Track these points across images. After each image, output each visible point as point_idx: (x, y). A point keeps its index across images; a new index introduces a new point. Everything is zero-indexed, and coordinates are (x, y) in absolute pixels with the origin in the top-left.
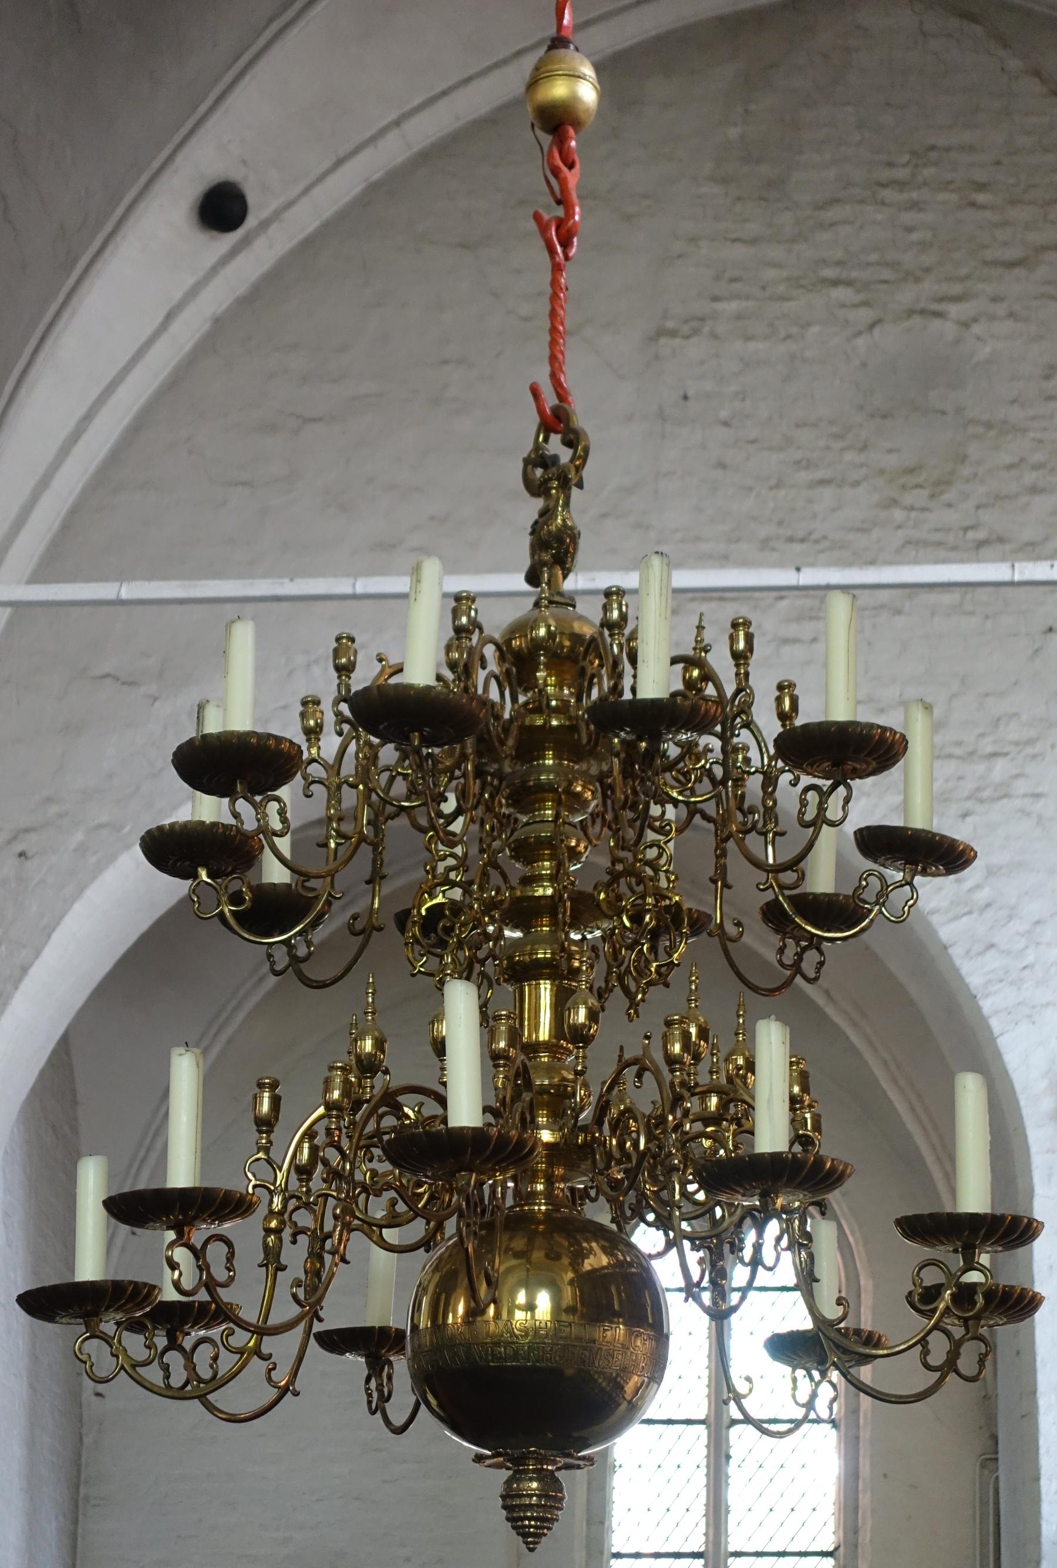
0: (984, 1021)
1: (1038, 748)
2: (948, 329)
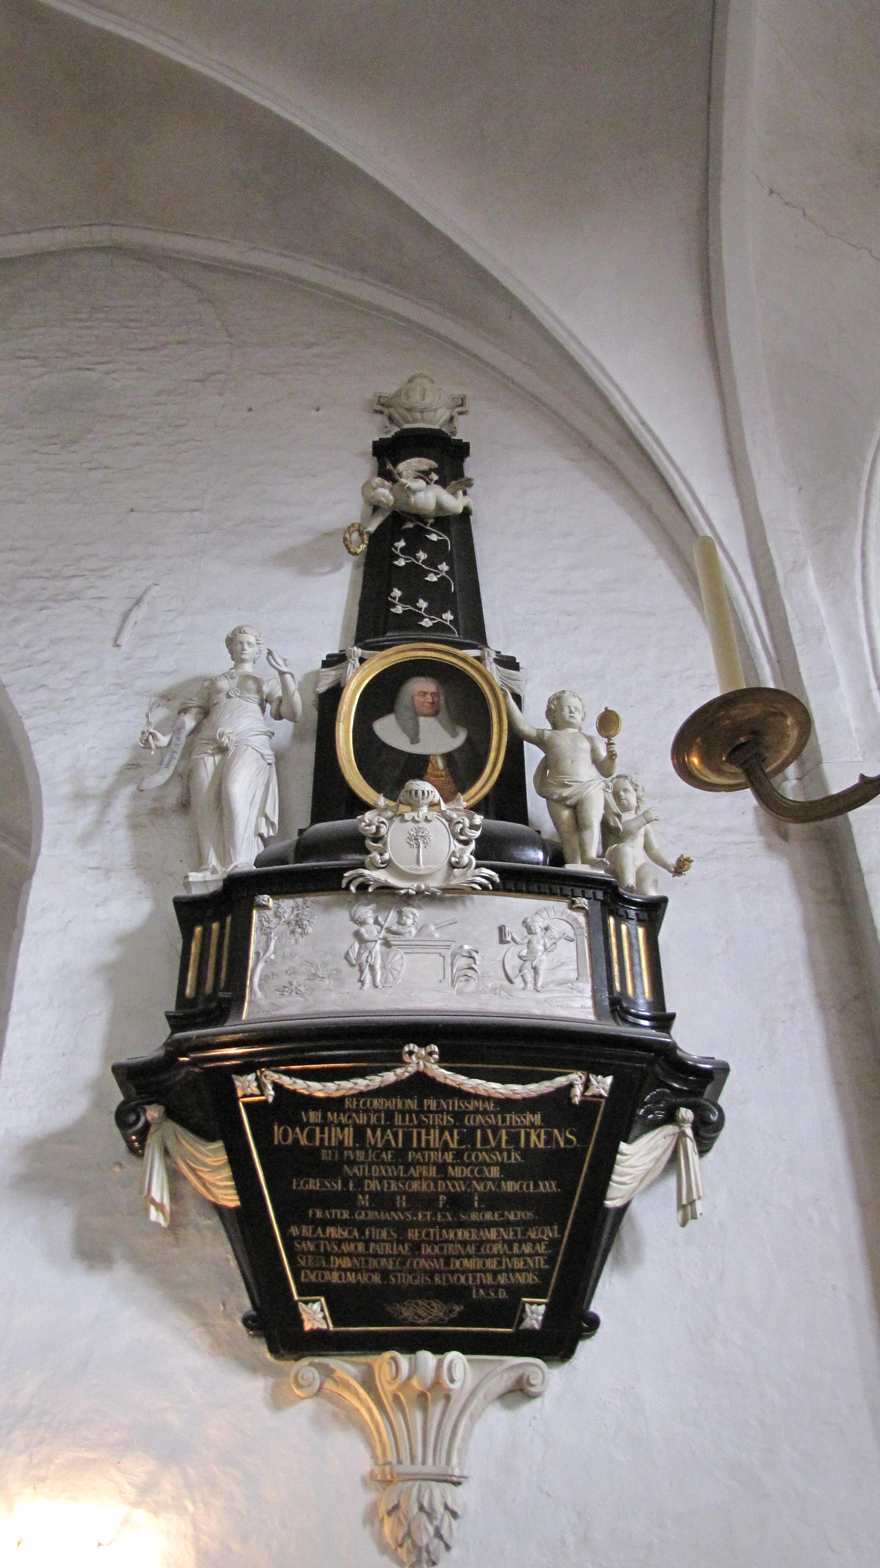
0: (24, 733)
1: (106, 573)
2: (94, 376)
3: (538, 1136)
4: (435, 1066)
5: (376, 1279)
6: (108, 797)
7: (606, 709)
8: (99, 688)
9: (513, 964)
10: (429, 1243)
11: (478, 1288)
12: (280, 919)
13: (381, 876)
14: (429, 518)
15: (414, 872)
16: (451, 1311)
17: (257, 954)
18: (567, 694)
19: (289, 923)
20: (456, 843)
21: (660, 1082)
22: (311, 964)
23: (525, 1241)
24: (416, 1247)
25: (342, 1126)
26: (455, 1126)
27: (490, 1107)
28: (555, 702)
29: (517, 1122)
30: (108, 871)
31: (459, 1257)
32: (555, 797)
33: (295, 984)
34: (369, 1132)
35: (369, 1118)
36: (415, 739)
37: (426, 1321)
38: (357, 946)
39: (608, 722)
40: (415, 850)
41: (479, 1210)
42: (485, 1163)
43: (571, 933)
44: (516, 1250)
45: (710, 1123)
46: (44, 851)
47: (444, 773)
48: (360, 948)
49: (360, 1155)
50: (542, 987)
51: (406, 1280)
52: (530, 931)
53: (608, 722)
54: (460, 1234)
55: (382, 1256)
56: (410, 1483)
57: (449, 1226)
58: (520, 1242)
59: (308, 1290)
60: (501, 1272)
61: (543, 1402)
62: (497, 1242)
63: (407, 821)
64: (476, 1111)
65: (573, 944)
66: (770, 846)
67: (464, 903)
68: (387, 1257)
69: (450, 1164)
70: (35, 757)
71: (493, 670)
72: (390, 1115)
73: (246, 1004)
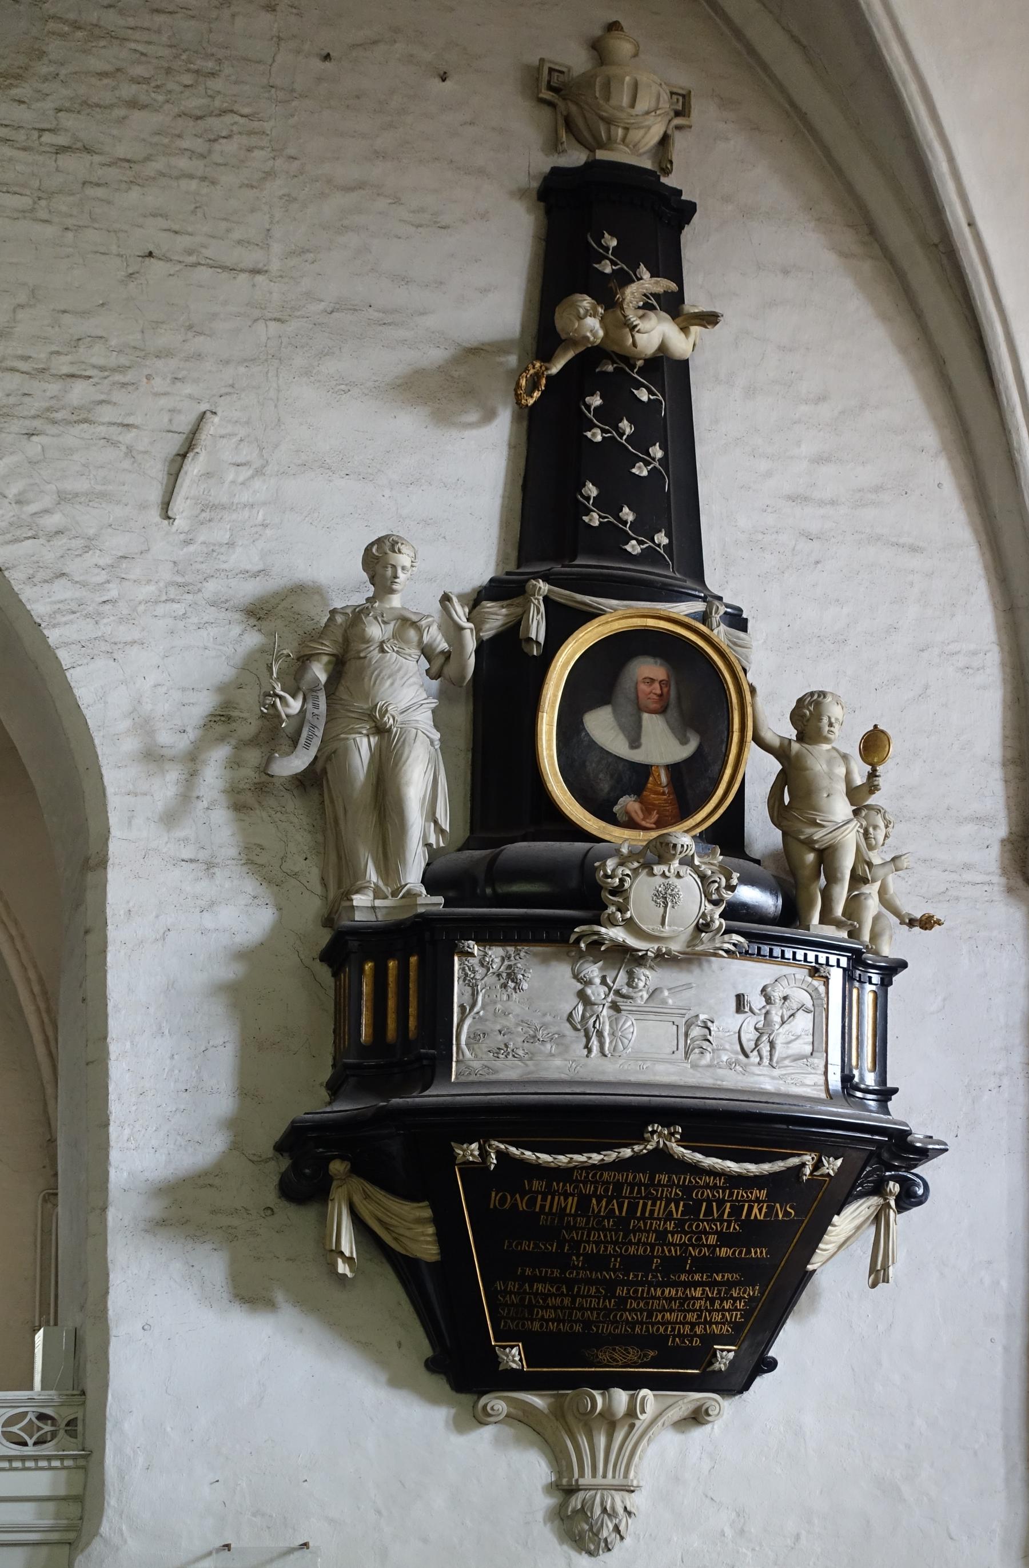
1: (128, 377)
3: (760, 1210)
4: (674, 1145)
5: (578, 1328)
6: (192, 760)
7: (876, 726)
8: (151, 588)
9: (749, 1037)
10: (635, 1299)
11: (674, 1336)
12: (488, 970)
13: (617, 934)
14: (639, 359)
15: (656, 934)
16: (645, 1355)
17: (462, 1007)
18: (829, 699)
19: (499, 975)
20: (707, 904)
21: (888, 1163)
22: (529, 1026)
23: (727, 1299)
24: (622, 1302)
25: (566, 1196)
26: (682, 1199)
27: (720, 1182)
28: (812, 708)
29: (742, 1196)
30: (210, 866)
31: (664, 1310)
32: (802, 837)
33: (511, 1046)
34: (594, 1201)
35: (596, 1188)
36: (635, 743)
37: (620, 1363)
38: (581, 1008)
39: (874, 745)
40: (662, 910)
41: (689, 1272)
42: (705, 1232)
43: (809, 1004)
44: (717, 1305)
45: (914, 1195)
46: (115, 832)
47: (666, 790)
48: (584, 1011)
49: (581, 1221)
50: (777, 1063)
51: (606, 1329)
52: (769, 1000)
53: (874, 745)
54: (667, 1291)
55: (587, 1309)
56: (593, 1492)
57: (663, 1285)
58: (722, 1300)
59: (506, 1336)
60: (699, 1324)
61: (713, 1428)
62: (701, 1299)
63: (655, 875)
64: (707, 1186)
65: (811, 1016)
66: (1010, 890)
67: (700, 965)
68: (592, 1310)
69: (670, 1232)
70: (75, 691)
71: (721, 633)
72: (618, 1186)
73: (454, 1064)
